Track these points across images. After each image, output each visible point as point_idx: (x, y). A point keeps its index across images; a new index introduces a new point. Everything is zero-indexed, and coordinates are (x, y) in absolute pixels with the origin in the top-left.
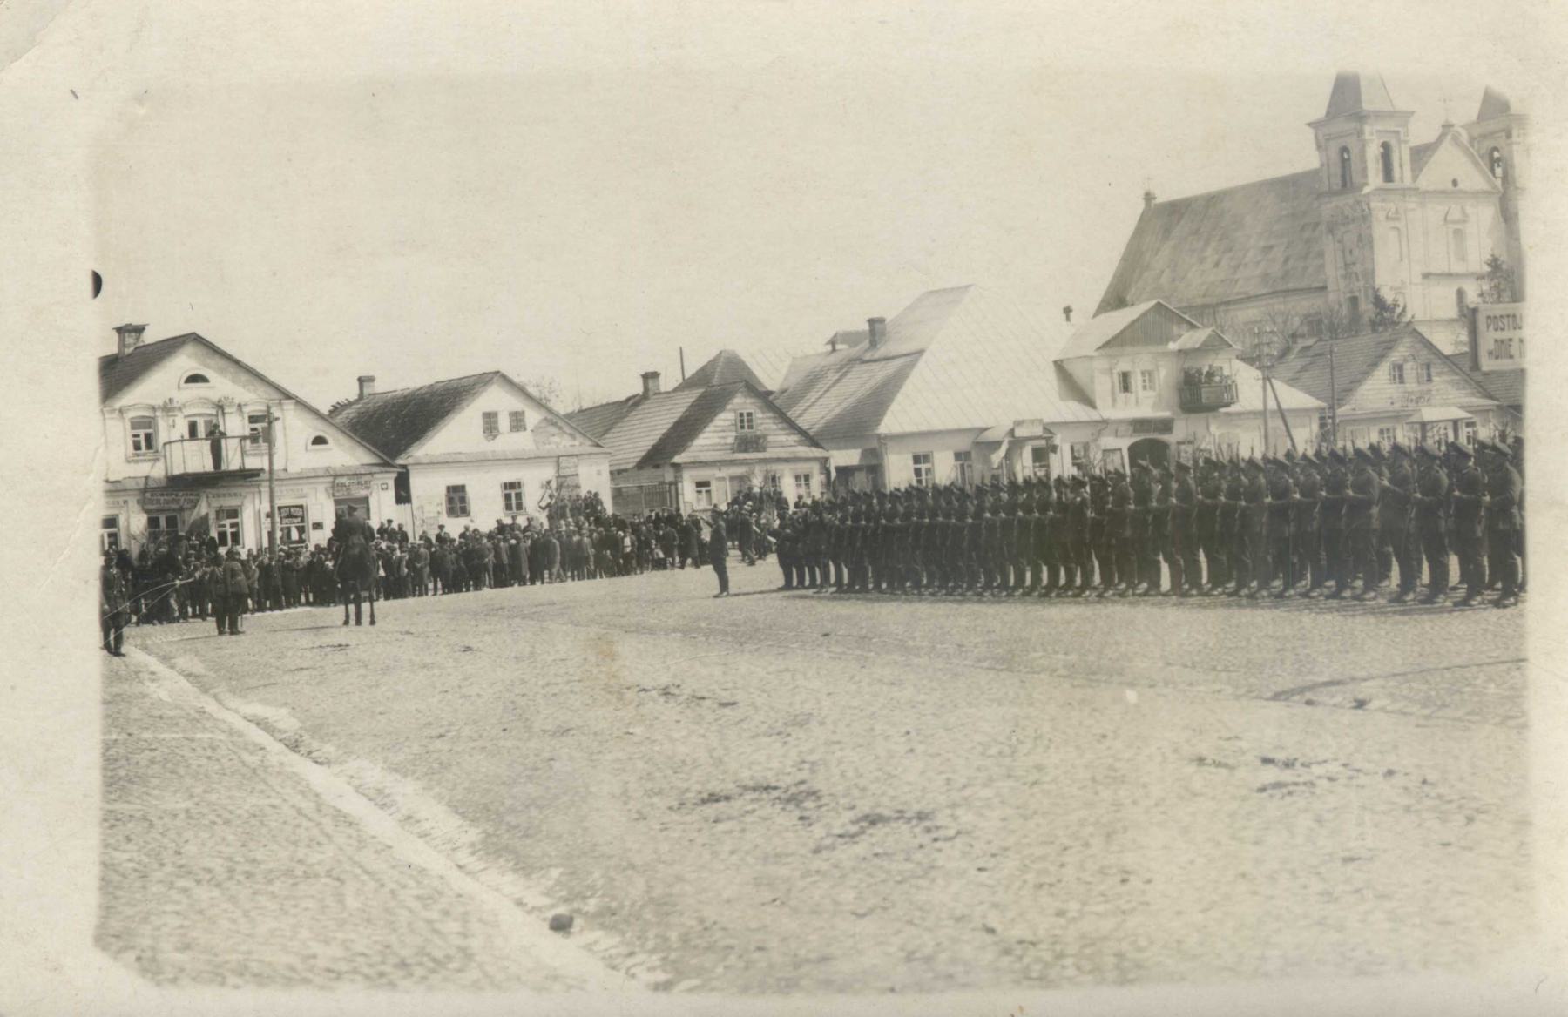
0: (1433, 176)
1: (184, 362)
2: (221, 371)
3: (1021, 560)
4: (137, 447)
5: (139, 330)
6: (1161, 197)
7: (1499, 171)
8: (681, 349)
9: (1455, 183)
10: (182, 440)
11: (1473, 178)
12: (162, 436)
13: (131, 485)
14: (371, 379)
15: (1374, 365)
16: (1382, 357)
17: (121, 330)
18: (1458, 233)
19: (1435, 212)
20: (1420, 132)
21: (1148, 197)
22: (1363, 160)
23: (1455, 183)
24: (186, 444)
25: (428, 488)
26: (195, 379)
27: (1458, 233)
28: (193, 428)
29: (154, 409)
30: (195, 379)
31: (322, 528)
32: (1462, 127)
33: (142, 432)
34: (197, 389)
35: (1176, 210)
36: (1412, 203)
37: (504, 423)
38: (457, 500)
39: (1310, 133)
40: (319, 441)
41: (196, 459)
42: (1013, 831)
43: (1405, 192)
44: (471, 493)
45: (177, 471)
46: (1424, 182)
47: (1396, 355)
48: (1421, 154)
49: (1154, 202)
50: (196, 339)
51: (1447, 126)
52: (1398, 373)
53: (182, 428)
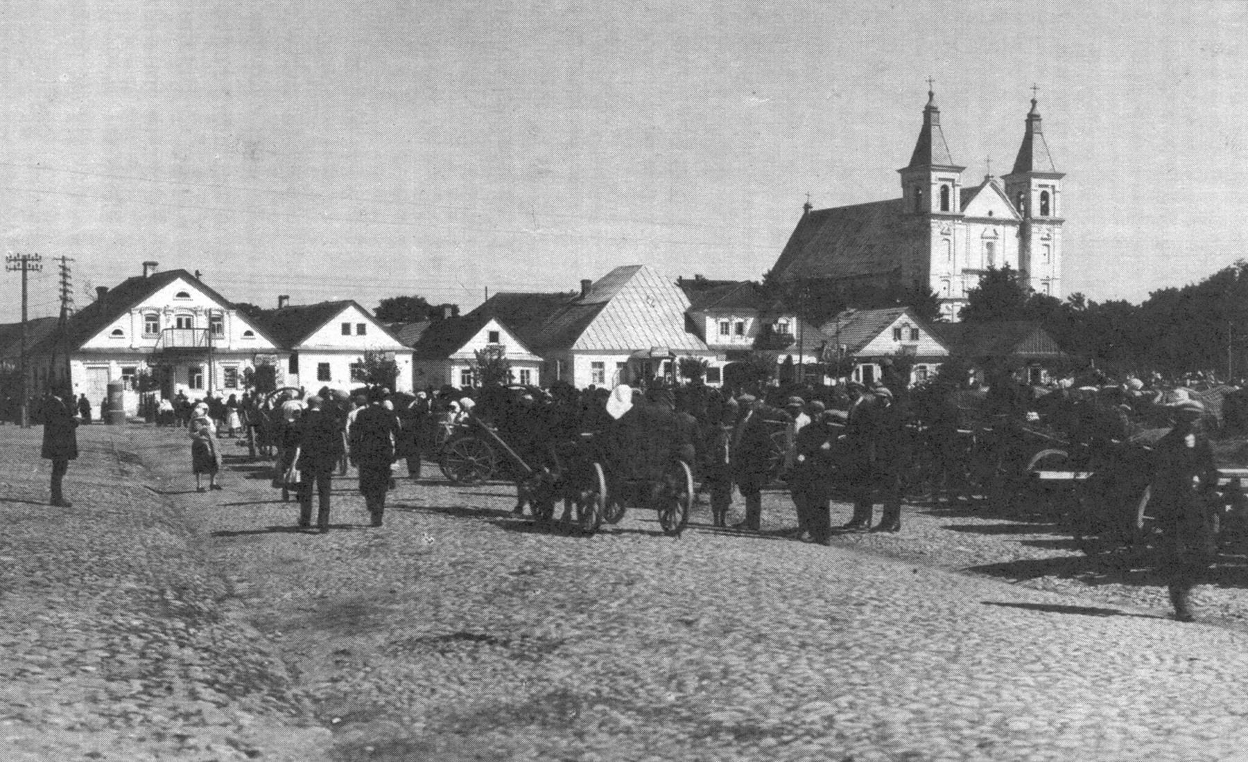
0: (976, 208)
1: (179, 285)
2: (196, 291)
3: (449, 429)
4: (148, 330)
5: (154, 264)
6: (816, 207)
7: (1022, 208)
8: (1032, 119)
9: (990, 213)
10: (173, 328)
11: (1004, 210)
12: (163, 325)
13: (143, 351)
14: (287, 297)
15: (882, 328)
16: (888, 323)
17: (145, 264)
18: (990, 246)
19: (977, 229)
20: (966, 180)
21: (807, 207)
22: (929, 194)
23: (990, 213)
24: (175, 331)
25: (309, 364)
26: (183, 295)
27: (990, 246)
28: (179, 321)
29: (158, 310)
30: (183, 295)
31: (327, 365)
32: (1002, 177)
33: (151, 323)
34: (183, 303)
35: (825, 215)
36: (960, 227)
37: (354, 330)
38: (324, 372)
39: (899, 176)
40: (248, 333)
41: (181, 340)
42: (1195, 723)
43: (954, 217)
44: (333, 370)
45: (170, 345)
46: (970, 212)
47: (896, 324)
48: (968, 195)
49: (810, 210)
50: (182, 274)
51: (987, 178)
52: (897, 334)
53: (174, 322)
